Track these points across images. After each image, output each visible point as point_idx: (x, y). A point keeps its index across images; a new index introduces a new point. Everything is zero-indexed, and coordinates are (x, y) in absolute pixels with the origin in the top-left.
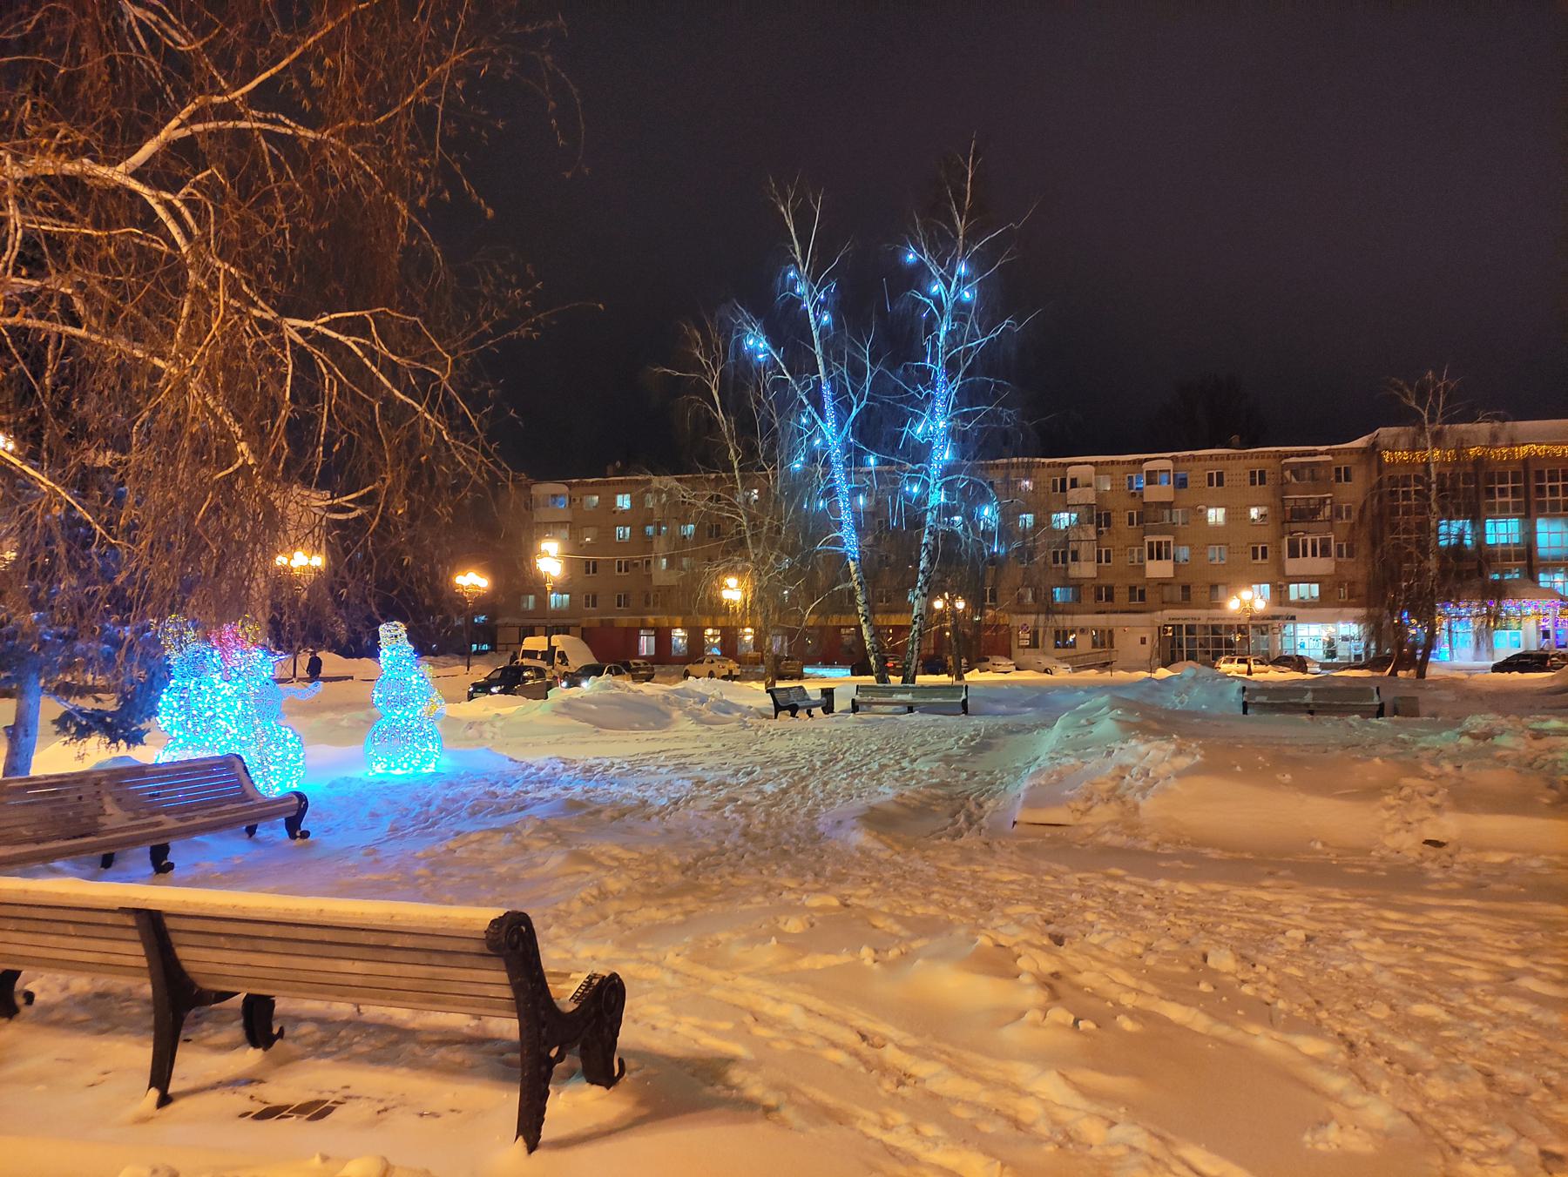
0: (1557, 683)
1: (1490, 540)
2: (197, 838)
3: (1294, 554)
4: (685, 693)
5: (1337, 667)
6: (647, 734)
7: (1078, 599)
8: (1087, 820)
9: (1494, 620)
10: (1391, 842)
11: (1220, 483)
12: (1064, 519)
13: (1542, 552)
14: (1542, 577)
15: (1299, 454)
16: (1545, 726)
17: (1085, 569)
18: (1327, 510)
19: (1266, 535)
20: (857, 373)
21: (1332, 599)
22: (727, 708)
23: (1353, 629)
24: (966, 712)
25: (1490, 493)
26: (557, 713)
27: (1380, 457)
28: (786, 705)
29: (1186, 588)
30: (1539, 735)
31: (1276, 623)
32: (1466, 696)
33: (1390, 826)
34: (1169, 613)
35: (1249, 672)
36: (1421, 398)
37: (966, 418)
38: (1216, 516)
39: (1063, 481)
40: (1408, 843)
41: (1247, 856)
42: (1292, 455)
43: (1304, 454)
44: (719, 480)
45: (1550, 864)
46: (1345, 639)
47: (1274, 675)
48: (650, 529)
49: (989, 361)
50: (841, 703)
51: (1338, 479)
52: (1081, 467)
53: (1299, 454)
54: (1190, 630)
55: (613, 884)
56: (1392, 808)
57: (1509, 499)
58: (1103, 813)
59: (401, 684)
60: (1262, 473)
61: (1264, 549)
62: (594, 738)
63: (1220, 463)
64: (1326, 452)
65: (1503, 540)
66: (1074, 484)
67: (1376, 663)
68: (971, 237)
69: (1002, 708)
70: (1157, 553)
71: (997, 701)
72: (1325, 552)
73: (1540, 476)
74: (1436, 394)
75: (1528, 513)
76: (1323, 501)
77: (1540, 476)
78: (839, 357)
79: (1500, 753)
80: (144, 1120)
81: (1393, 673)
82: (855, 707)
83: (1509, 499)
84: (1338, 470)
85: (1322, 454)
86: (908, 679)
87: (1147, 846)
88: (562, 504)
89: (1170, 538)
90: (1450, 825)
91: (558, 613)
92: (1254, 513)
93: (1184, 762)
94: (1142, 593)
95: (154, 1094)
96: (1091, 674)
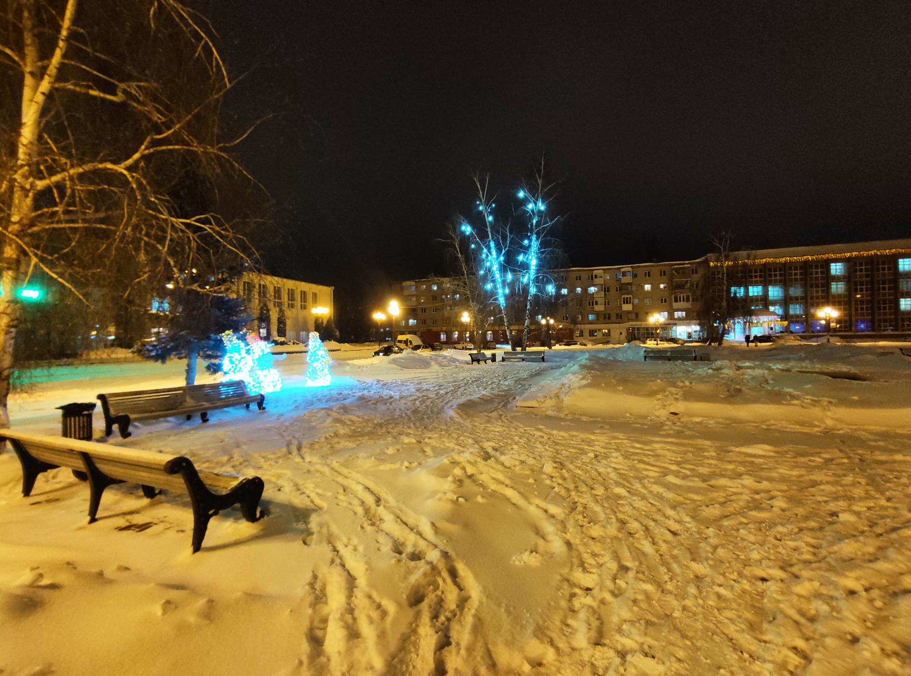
0: (773, 346)
1: (751, 294)
2: (226, 409)
3: (676, 301)
4: (439, 356)
5: (692, 342)
6: (419, 371)
7: (598, 319)
8: (543, 405)
9: (748, 324)
10: (657, 413)
11: (649, 276)
12: (592, 289)
13: (770, 298)
14: (770, 307)
15: (678, 264)
16: (743, 365)
17: (600, 308)
18: (689, 285)
19: (666, 294)
20: (504, 238)
21: (687, 319)
22: (454, 360)
23: (698, 328)
24: (543, 361)
25: (770, 276)
26: (390, 363)
27: (709, 265)
28: (475, 359)
29: (637, 314)
30: (739, 368)
31: (669, 326)
32: (736, 353)
33: (657, 407)
34: (631, 323)
35: (657, 344)
36: (721, 240)
37: (542, 253)
38: (648, 287)
39: (592, 276)
40: (663, 414)
41: (599, 419)
42: (676, 264)
43: (680, 264)
44: (460, 279)
45: (718, 423)
46: (695, 332)
47: (666, 345)
48: (444, 297)
49: (552, 232)
50: (498, 358)
51: (693, 273)
52: (598, 271)
53: (678, 264)
54: (638, 329)
55: (342, 432)
56: (659, 400)
57: (758, 279)
58: (550, 403)
59: (316, 354)
60: (664, 272)
61: (665, 300)
62: (400, 372)
63: (649, 269)
64: (688, 264)
65: (756, 294)
66: (596, 277)
67: (703, 340)
68: (544, 186)
69: (557, 359)
70: (626, 301)
71: (556, 357)
72: (688, 300)
73: (751, 271)
74: (726, 241)
75: (765, 284)
76: (687, 282)
77: (770, 270)
78: (498, 232)
79: (721, 376)
80: (81, 528)
81: (710, 344)
82: (503, 360)
83: (758, 279)
84: (693, 270)
85: (687, 264)
86: (524, 349)
87: (562, 415)
88: (413, 288)
89: (631, 296)
90: (680, 407)
91: (412, 327)
92: (662, 286)
93: (584, 382)
94: (621, 316)
95: (88, 518)
96: (600, 346)
